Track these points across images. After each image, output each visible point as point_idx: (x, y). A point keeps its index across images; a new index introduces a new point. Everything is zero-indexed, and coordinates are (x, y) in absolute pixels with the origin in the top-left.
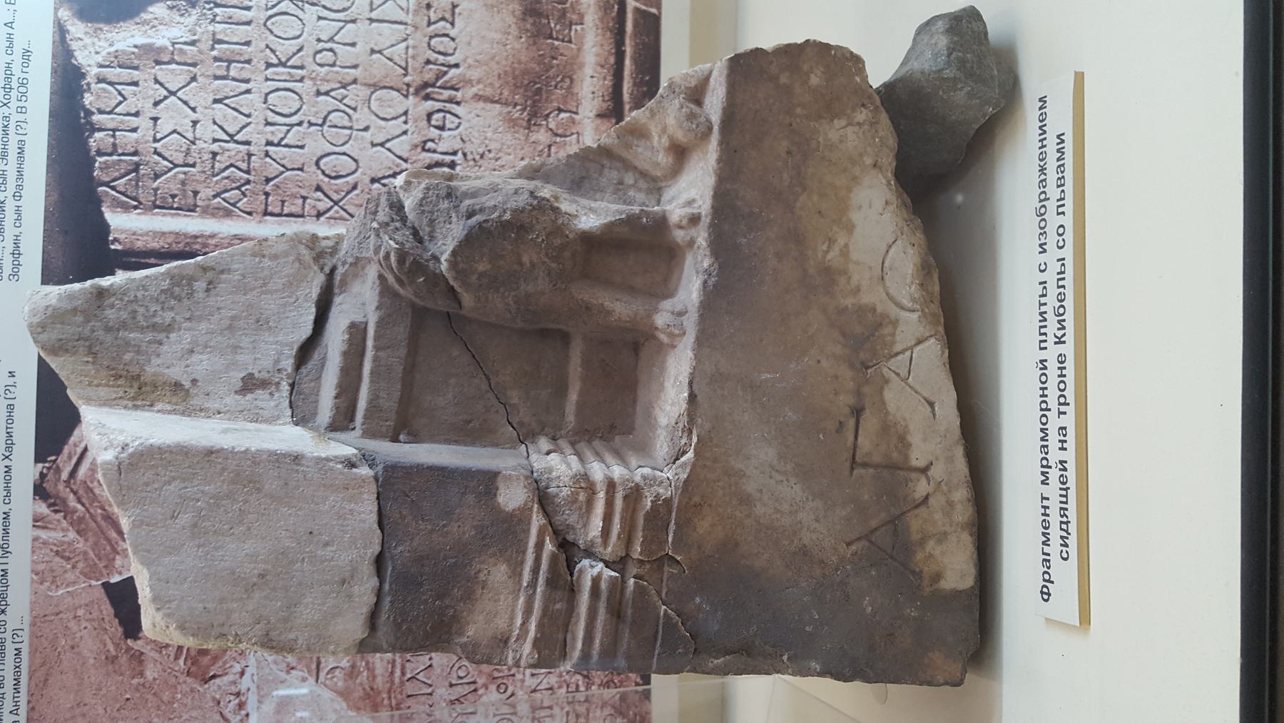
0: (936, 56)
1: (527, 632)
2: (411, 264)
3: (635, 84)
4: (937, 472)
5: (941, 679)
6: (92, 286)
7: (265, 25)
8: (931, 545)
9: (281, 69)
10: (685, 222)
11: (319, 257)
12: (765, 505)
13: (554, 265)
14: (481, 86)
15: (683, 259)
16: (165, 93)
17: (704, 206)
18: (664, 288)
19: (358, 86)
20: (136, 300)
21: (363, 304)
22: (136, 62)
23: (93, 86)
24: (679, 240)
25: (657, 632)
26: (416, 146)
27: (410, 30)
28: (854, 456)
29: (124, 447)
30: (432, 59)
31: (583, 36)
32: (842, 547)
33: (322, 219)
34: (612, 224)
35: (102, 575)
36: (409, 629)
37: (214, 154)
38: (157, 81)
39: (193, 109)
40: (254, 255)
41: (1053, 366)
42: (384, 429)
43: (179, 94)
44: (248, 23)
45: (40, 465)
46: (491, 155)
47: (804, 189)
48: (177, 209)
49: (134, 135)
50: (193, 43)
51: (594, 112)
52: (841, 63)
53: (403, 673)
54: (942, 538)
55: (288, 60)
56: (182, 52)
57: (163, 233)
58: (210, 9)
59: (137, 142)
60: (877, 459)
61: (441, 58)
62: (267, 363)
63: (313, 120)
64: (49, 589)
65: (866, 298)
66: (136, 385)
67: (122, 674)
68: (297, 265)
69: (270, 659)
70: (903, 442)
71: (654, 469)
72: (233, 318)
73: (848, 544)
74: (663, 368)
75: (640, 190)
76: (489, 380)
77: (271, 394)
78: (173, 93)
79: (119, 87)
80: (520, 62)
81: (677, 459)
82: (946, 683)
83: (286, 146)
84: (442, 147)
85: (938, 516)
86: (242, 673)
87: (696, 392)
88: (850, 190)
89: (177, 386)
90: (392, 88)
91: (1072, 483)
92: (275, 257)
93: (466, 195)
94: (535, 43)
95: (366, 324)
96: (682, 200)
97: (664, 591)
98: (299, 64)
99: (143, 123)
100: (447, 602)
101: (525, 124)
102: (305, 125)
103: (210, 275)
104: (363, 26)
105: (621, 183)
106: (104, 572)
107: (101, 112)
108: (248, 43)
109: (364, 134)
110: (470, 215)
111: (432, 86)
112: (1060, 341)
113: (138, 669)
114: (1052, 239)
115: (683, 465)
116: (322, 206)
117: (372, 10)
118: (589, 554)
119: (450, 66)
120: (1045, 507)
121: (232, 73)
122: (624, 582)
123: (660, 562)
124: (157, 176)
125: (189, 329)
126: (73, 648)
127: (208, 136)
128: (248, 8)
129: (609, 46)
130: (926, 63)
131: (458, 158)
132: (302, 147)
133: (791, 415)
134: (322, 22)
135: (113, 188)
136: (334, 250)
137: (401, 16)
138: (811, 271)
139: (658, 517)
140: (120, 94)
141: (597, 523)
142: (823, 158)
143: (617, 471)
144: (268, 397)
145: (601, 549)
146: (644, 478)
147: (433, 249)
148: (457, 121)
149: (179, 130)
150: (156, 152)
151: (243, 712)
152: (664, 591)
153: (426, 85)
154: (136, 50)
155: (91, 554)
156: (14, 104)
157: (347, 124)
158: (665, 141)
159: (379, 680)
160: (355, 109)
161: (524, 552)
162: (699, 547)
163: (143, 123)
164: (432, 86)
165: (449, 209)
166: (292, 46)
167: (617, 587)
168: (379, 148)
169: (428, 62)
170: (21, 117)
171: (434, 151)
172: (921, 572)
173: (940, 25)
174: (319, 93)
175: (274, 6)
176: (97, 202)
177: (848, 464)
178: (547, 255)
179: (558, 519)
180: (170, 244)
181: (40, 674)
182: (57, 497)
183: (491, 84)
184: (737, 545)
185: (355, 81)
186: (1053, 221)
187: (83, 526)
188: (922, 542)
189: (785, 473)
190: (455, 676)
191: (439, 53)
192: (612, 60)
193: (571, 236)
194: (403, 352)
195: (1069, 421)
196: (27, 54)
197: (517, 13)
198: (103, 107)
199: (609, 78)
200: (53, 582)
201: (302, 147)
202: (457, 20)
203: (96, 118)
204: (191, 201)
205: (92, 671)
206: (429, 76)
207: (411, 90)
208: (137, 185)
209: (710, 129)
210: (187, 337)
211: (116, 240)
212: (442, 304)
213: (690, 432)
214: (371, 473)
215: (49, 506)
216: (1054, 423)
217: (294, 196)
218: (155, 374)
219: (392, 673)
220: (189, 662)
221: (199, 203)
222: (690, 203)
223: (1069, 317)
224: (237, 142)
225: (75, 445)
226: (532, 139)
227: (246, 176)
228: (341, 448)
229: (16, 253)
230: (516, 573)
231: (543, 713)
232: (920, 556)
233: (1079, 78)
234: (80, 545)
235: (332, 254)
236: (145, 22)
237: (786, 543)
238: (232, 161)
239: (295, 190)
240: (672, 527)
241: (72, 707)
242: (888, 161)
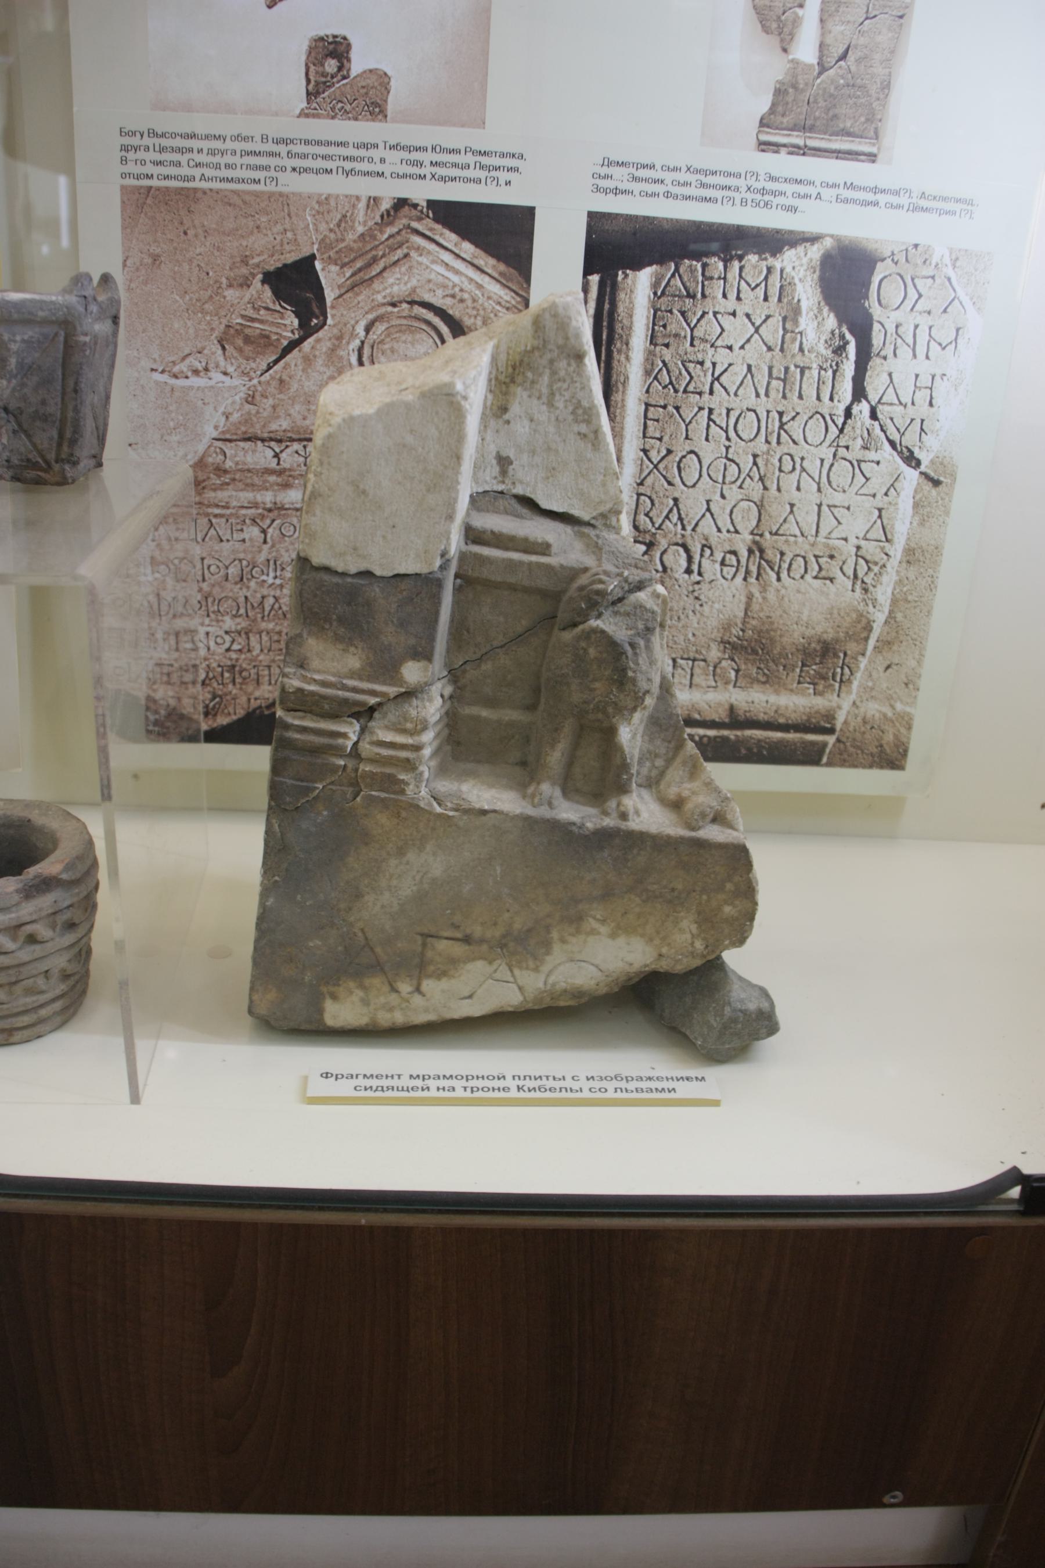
0: (742, 1001)
1: (309, 684)
2: (595, 601)
3: (759, 741)
4: (417, 1000)
5: (255, 997)
6: (586, 347)
7: (817, 412)
8: (360, 993)
9: (777, 424)
10: (622, 808)
11: (603, 516)
12: (397, 866)
13: (592, 706)
14: (760, 600)
15: (592, 806)
16: (757, 324)
17: (634, 824)
18: (569, 789)
19: (761, 491)
20: (573, 382)
21: (565, 552)
22: (785, 300)
23: (764, 263)
24: (609, 804)
25: (302, 781)
26: (707, 540)
27: (811, 539)
28: (432, 936)
29: (465, 398)
30: (785, 558)
31: (803, 695)
32: (360, 924)
33: (642, 454)
34: (623, 752)
35: (322, 254)
36: (315, 596)
37: (702, 363)
38: (768, 317)
39: (742, 347)
40: (606, 469)
41: (501, 1084)
42: (466, 567)
43: (756, 336)
44: (818, 398)
45: (425, 204)
46: (698, 607)
47: (644, 901)
48: (653, 329)
49: (720, 296)
50: (801, 350)
51: (735, 703)
52: (740, 929)
53: (216, 516)
54: (365, 1002)
55: (786, 431)
56: (794, 340)
57: (631, 316)
58: (831, 366)
59: (714, 298)
60: (429, 954)
61: (785, 566)
62: (520, 474)
63: (731, 450)
64: (312, 209)
65: (557, 948)
66: (507, 380)
67: (231, 269)
68: (597, 500)
69: (237, 398)
70: (442, 974)
71: (428, 780)
72: (557, 451)
73: (362, 930)
74: (508, 787)
75: (650, 771)
76: (502, 647)
77: (495, 478)
78: (757, 331)
79: (763, 285)
80: (781, 636)
81: (435, 799)
82: (251, 1001)
83: (708, 426)
84: (706, 563)
85: (382, 1000)
86: (225, 374)
87: (488, 816)
88: (642, 936)
89: (504, 409)
90: (759, 520)
91: (412, 1094)
92: (604, 485)
93: (648, 641)
94: (798, 650)
95: (550, 555)
96: (640, 806)
97: (334, 788)
98: (782, 440)
99: (731, 304)
100: (335, 624)
101: (726, 638)
102: (727, 443)
103: (592, 436)
104: (815, 498)
105: (656, 756)
106: (326, 256)
107: (741, 269)
108: (800, 397)
109: (719, 494)
110: (632, 645)
111: (760, 557)
112: (519, 1088)
113: (235, 283)
114: (597, 1084)
115: (431, 805)
116: (655, 457)
117: (829, 506)
118: (363, 730)
119: (778, 574)
120: (392, 1077)
121: (774, 383)
122: (341, 756)
123: (355, 785)
124: (683, 313)
125: (549, 419)
126: (258, 227)
127: (717, 359)
128: (831, 399)
129: (794, 718)
130: (736, 993)
131: (695, 577)
132: (707, 439)
133: (466, 889)
134: (818, 462)
135: (673, 275)
136: (608, 527)
137: (823, 532)
138: (580, 907)
139: (391, 783)
140: (757, 285)
141: (389, 737)
142: (668, 916)
143: (427, 752)
144: (494, 475)
145: (368, 739)
146: (421, 774)
147: (607, 614)
148: (729, 577)
149: (725, 334)
150: (704, 313)
151: (189, 374)
152: (334, 788)
153: (762, 551)
154: (796, 300)
155: (342, 245)
156: (749, 196)
157: (727, 480)
158: (686, 793)
159: (212, 494)
160: (740, 487)
161: (368, 681)
162: (366, 815)
163: (731, 304)
164: (760, 557)
165: (637, 629)
166: (798, 436)
167: (338, 751)
168: (705, 506)
169: (782, 554)
170: (738, 201)
171: (702, 556)
172: (339, 985)
173: (765, 1005)
174: (755, 456)
175: (833, 421)
176: (661, 261)
177: (426, 931)
178: (600, 701)
179: (391, 706)
180: (621, 322)
181: (235, 199)
182: (395, 217)
183: (762, 610)
184: (366, 844)
185: (765, 488)
186: (610, 1086)
187: (368, 239)
188: (362, 987)
189: (421, 882)
190: (212, 562)
191: (790, 565)
192: (782, 720)
193: (614, 720)
194: (526, 583)
195: (460, 1093)
196: (792, 209)
197: (825, 636)
198: (745, 271)
199: (766, 718)
200: (318, 212)
201: (707, 439)
202: (819, 581)
203: (736, 264)
204: (660, 341)
205: (236, 244)
206: (769, 554)
207: (757, 538)
208: (675, 296)
209: (693, 829)
210: (543, 418)
211: (626, 276)
212: (563, 616)
213: (456, 810)
214: (436, 569)
215: (388, 211)
216: (458, 1084)
217: (663, 430)
218: (515, 394)
219: (217, 506)
220: (238, 327)
221: (658, 348)
222: (637, 813)
223: (538, 1095)
224: (712, 384)
225: (441, 235)
226: (712, 645)
227: (682, 389)
228: (455, 542)
229: (616, 191)
230: (352, 674)
231: (173, 642)
232: (352, 984)
233: (716, 1103)
234: (350, 236)
235: (605, 525)
236: (820, 310)
237: (366, 882)
238: (695, 378)
239: (668, 431)
240: (383, 795)
241: (203, 226)
242: (664, 966)
